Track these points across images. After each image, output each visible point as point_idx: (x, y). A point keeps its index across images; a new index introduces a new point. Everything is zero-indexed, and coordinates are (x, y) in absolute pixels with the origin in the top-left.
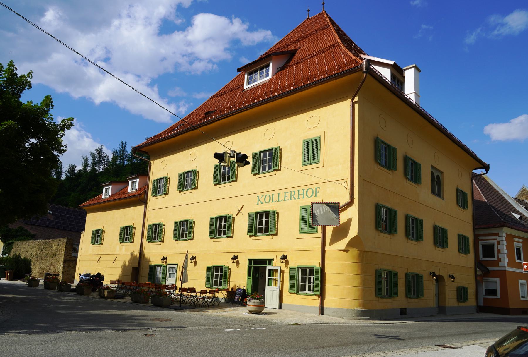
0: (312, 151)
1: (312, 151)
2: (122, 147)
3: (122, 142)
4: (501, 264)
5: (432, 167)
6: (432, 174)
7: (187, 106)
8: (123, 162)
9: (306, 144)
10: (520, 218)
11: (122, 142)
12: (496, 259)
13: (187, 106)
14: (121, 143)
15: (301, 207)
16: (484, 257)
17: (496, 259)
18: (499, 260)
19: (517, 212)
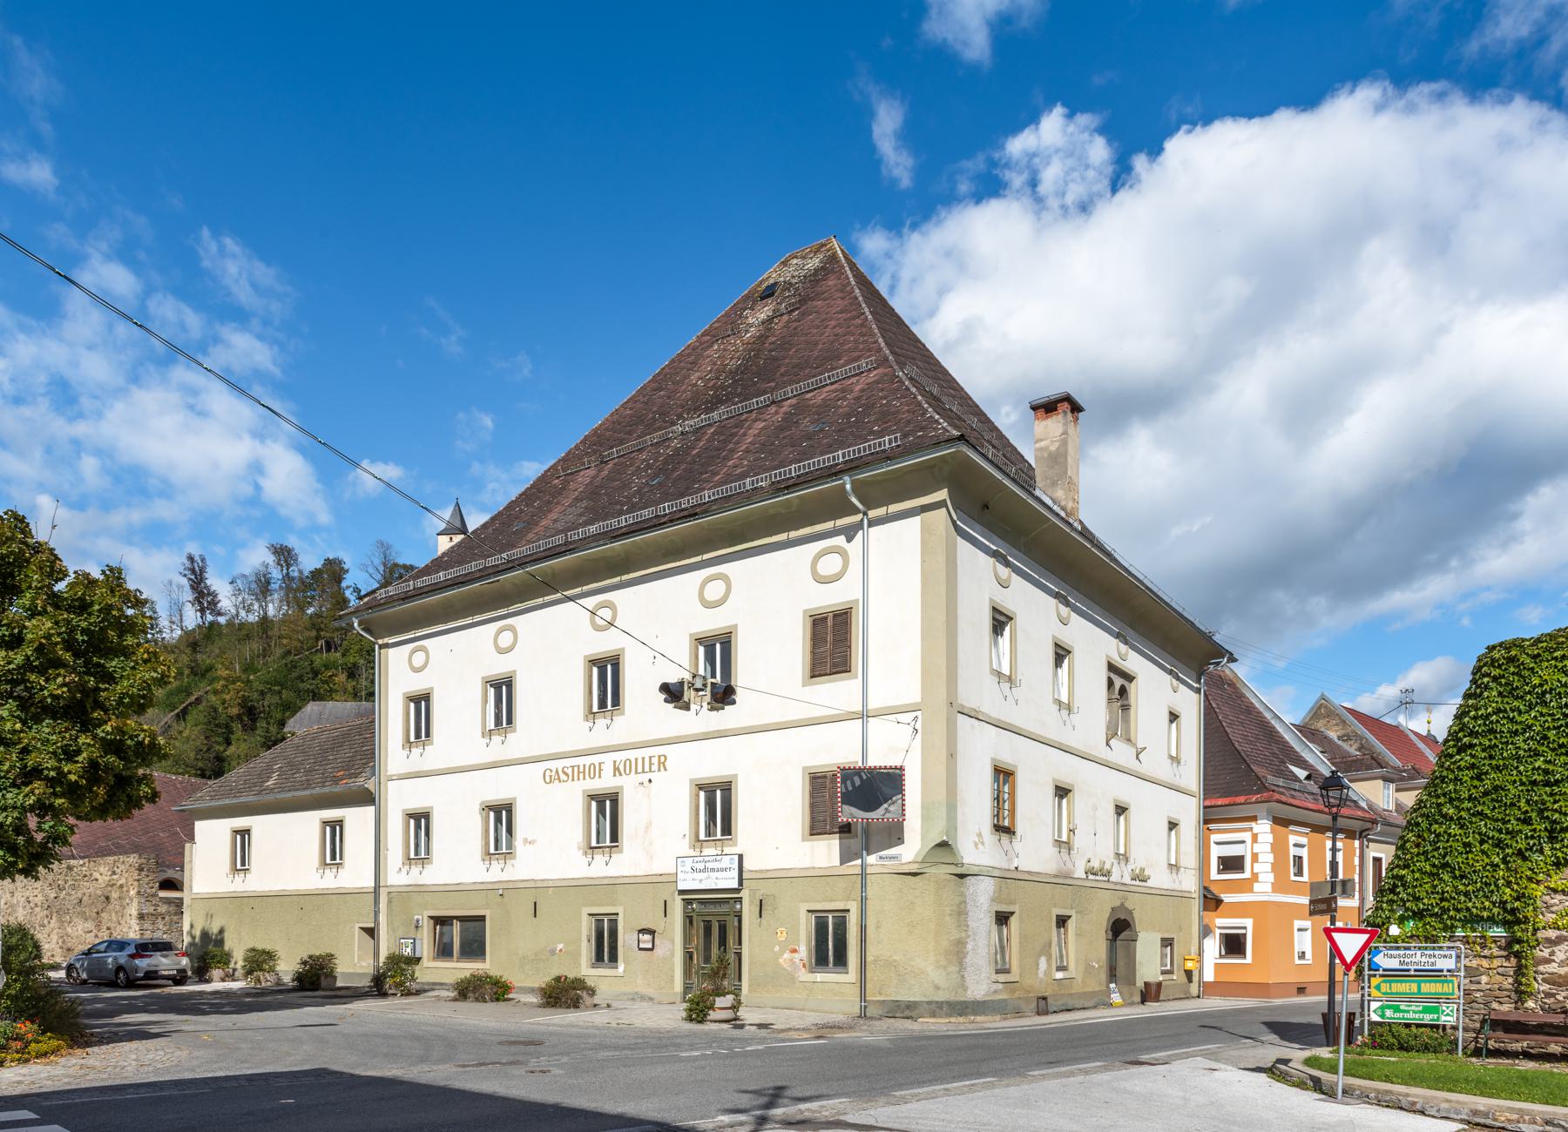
0: (832, 643)
1: (832, 643)
2: (193, 571)
3: (191, 559)
4: (1257, 887)
5: (1112, 668)
6: (1110, 683)
7: (476, 467)
8: (853, 784)
9: (614, 958)
10: (1308, 778)
11: (191, 559)
12: (1247, 874)
13: (476, 467)
14: (188, 564)
15: (804, 769)
16: (1219, 872)
17: (1247, 874)
18: (1255, 877)
19: (1302, 763)
